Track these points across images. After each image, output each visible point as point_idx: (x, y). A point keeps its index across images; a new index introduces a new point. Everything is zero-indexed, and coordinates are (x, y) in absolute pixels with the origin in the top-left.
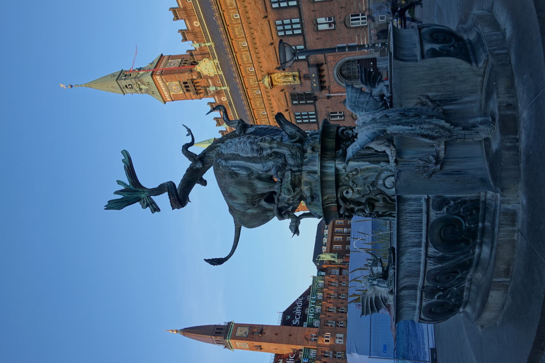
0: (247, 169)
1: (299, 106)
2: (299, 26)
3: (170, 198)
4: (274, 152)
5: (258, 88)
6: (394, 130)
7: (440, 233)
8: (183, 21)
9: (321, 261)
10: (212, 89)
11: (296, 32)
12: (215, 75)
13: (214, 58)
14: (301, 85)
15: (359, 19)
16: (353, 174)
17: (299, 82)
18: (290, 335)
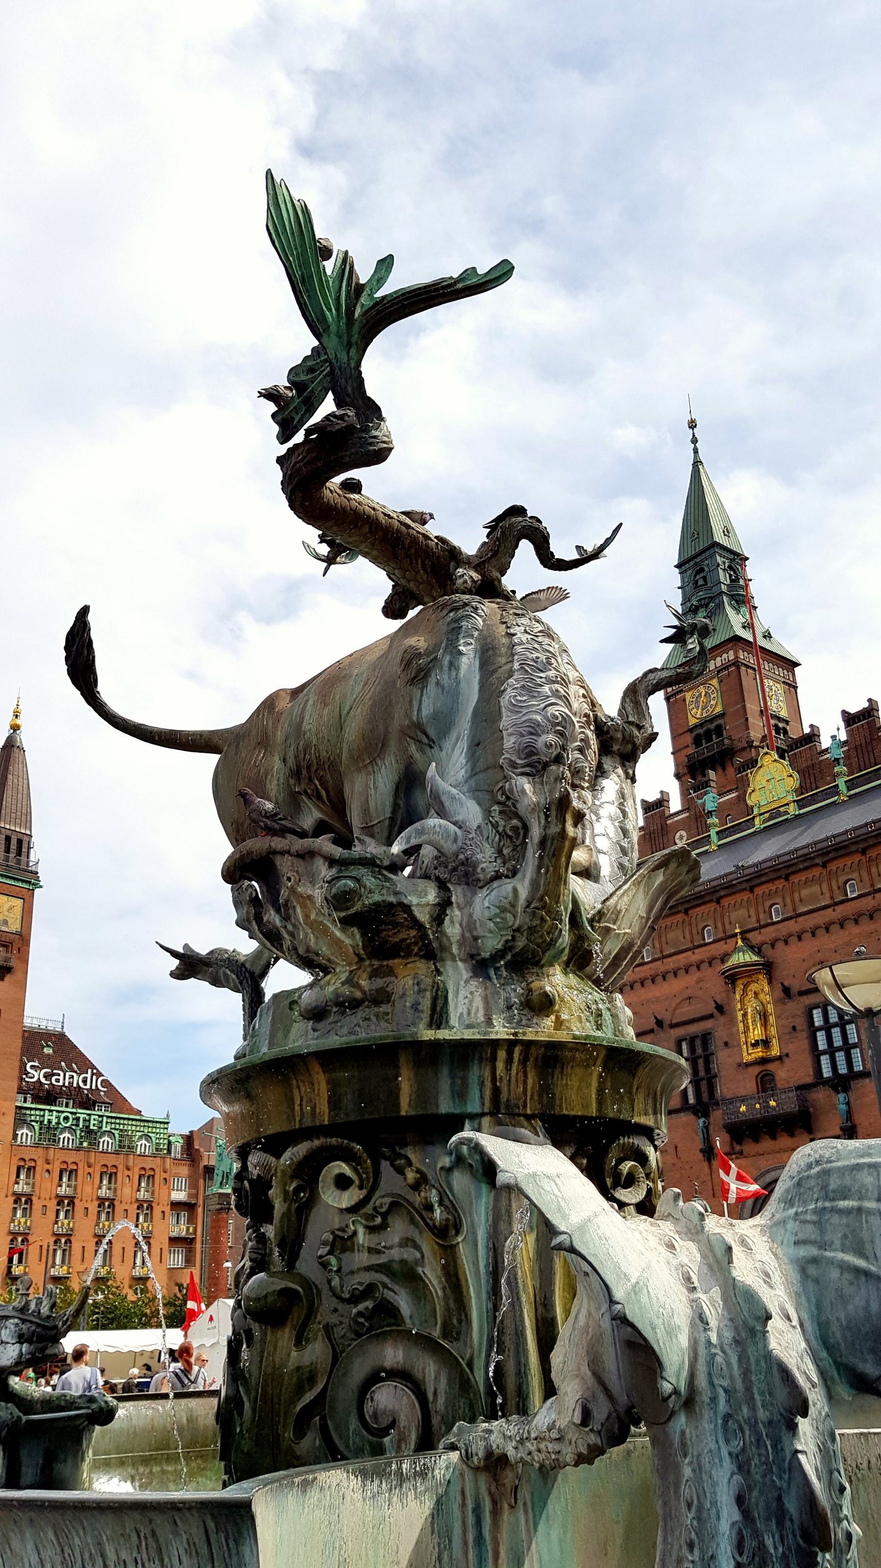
0: (445, 721)
2: (843, 1069)
4: (526, 828)
5: (721, 935)
6: (698, 1469)
13: (801, 804)
14: (739, 1065)
16: (429, 1208)
17: (747, 1058)
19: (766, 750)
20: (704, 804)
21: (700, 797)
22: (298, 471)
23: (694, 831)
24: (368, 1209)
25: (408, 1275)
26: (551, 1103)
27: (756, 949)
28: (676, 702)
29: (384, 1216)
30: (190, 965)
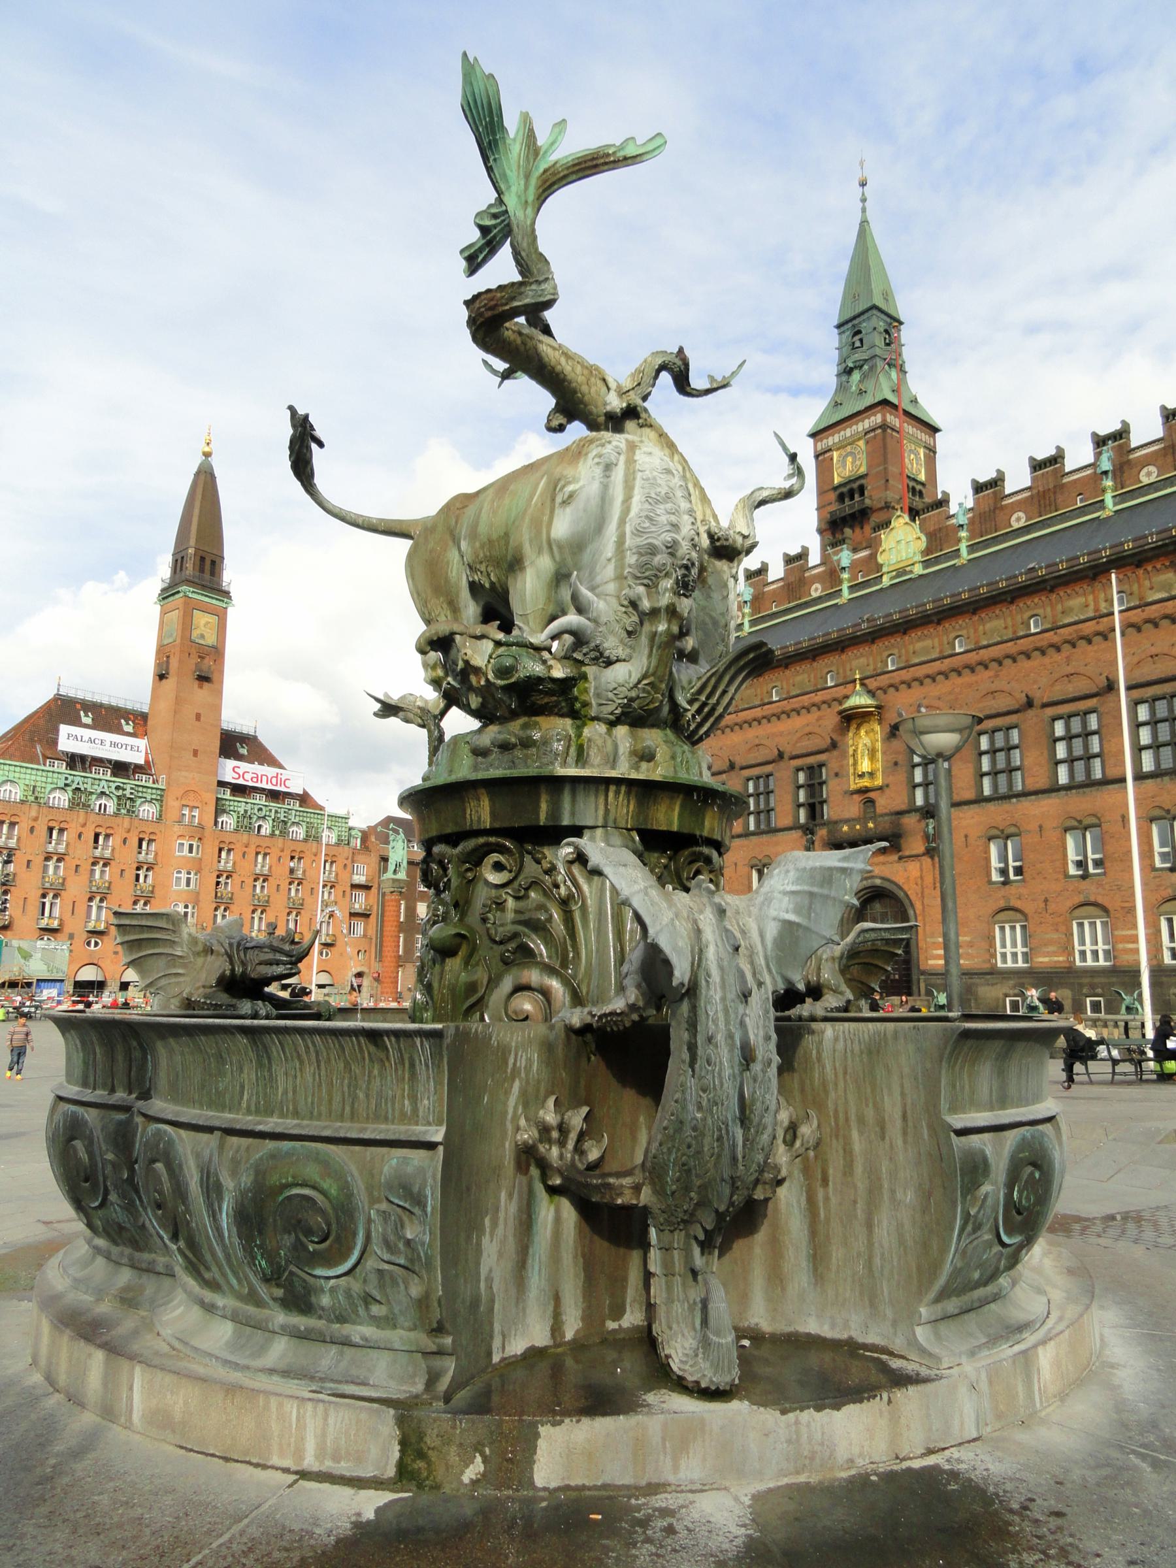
1: (791, 788)
3: (501, 288)
7: (304, 1185)
8: (1028, 484)
9: (387, 836)
10: (845, 557)
11: (986, 782)
12: (879, 567)
13: (926, 564)
15: (1014, 945)
18: (195, 753)
19: (899, 513)
20: (839, 561)
21: (836, 553)
22: (481, 314)
23: (828, 584)
24: (516, 884)
25: (540, 928)
26: (646, 819)
27: (871, 693)
28: (824, 460)
29: (527, 889)
30: (388, 709)
